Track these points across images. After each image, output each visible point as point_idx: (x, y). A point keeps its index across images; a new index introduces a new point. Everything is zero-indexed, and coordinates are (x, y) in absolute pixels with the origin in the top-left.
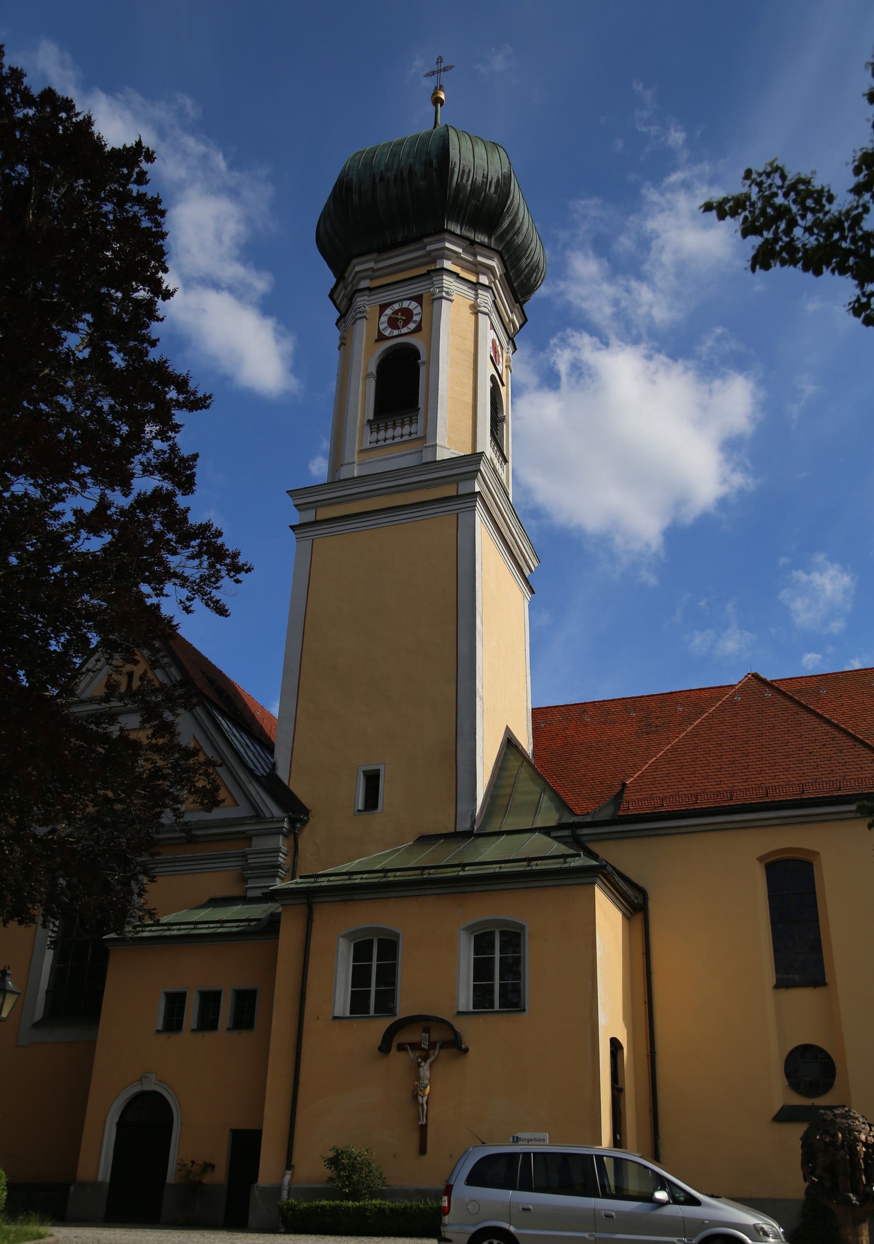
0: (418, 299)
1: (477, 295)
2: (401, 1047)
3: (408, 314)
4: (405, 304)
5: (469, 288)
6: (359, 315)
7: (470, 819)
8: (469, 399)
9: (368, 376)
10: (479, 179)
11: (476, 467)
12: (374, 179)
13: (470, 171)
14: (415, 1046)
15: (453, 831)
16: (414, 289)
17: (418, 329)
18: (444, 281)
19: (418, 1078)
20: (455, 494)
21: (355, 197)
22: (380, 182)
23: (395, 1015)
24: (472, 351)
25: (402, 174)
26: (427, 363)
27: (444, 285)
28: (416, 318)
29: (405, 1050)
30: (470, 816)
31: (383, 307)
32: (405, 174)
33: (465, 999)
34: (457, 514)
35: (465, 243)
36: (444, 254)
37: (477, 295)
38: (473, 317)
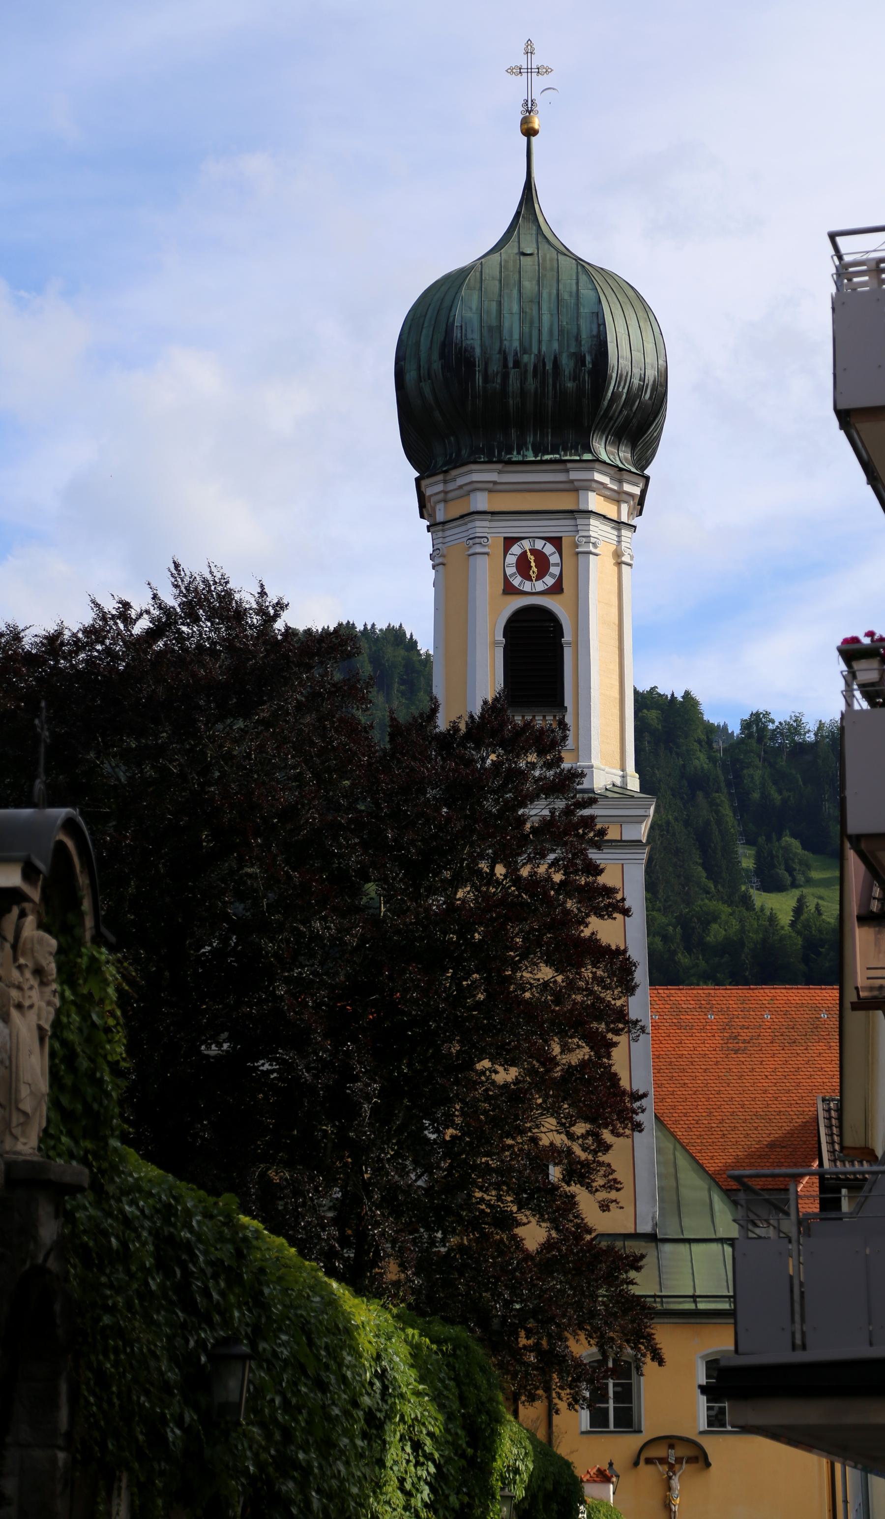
0: (556, 542)
1: (619, 536)
2: (649, 1461)
3: (542, 558)
4: (539, 545)
5: (613, 528)
6: (479, 549)
7: (651, 1221)
8: (617, 695)
9: (495, 643)
10: (636, 382)
11: (646, 812)
12: (505, 360)
13: (627, 374)
14: (663, 1461)
15: (632, 1231)
16: (553, 527)
17: (557, 589)
18: (591, 528)
19: (669, 1488)
20: (619, 839)
21: (479, 379)
22: (514, 367)
23: (640, 1431)
24: (617, 622)
25: (544, 364)
26: (576, 644)
27: (592, 534)
28: (555, 570)
29: (654, 1464)
30: (650, 1218)
31: (509, 542)
32: (549, 367)
33: (703, 1425)
34: (623, 864)
35: (612, 471)
36: (589, 486)
37: (619, 536)
38: (616, 568)
